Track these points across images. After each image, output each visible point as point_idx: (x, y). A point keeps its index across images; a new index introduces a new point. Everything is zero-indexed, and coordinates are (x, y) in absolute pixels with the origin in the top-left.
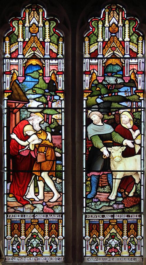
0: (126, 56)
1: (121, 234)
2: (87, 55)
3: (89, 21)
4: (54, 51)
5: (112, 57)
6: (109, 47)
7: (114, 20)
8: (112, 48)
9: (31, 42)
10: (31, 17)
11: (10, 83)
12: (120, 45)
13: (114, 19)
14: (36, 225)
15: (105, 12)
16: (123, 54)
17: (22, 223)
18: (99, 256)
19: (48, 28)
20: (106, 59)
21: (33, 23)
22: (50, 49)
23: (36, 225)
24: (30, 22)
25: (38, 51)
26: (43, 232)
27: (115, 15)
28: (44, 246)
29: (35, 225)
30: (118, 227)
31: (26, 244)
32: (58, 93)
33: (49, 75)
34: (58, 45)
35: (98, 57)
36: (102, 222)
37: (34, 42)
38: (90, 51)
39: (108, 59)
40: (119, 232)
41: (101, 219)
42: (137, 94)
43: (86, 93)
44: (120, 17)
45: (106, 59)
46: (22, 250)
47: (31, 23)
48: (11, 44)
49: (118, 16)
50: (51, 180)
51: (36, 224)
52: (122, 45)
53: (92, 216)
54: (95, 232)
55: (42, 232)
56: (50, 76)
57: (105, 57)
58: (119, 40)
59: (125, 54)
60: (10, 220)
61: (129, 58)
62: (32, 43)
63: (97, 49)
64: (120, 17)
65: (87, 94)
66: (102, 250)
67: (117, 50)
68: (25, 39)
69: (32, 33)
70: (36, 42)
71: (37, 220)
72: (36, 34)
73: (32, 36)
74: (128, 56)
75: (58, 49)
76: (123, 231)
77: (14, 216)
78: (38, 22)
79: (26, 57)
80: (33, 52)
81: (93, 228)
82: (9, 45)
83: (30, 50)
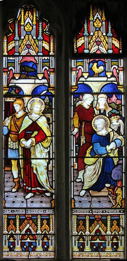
0: (39, 54)
1: (36, 229)
2: (6, 53)
3: (9, 21)
4: (46, 48)
5: (27, 55)
6: (25, 44)
7: (28, 20)
8: (97, 43)
9: (26, 40)
10: (95, 12)
11: (76, 78)
12: (104, 40)
13: (28, 18)
14: (99, 220)
15: (20, 13)
16: (37, 52)
17: (38, 218)
18: (119, 251)
19: (42, 26)
20: (22, 57)
21: (28, 23)
22: (43, 47)
23: (30, 220)
24: (25, 22)
25: (101, 46)
26: (36, 227)
27: (30, 15)
28: (37, 241)
29: (28, 220)
30: (33, 222)
31: (90, 240)
32: (119, 88)
33: (111, 70)
34: (49, 43)
35: (15, 54)
36: (40, 217)
37: (28, 40)
38: (76, 45)
39: (23, 56)
40: (103, 228)
41: (17, 214)
42: (50, 91)
43: (5, 90)
44: (34, 17)
45: (22, 57)
46: (108, 247)
47: (26, 23)
48: (8, 43)
49: (32, 16)
50: (17, 175)
51: (29, 219)
52: (36, 44)
53: (106, 212)
54: (81, 227)
55: (35, 228)
56: (43, 72)
57: (21, 54)
58: (103, 35)
59: (38, 52)
60: (76, 216)
61: (42, 56)
62: (27, 40)
63: (84, 43)
64: (34, 17)
65: (6, 91)
66: (40, 245)
67: (102, 45)
68: (90, 33)
69: (96, 28)
70: (30, 40)
71: (100, 216)
72: (30, 32)
73: (27, 34)
74: (41, 54)
75: (50, 46)
76: (37, 226)
77: (33, 211)
78: (32, 22)
79: (21, 54)
80: (97, 47)
81: (113, 224)
82: (4, 43)
83: (95, 45)
